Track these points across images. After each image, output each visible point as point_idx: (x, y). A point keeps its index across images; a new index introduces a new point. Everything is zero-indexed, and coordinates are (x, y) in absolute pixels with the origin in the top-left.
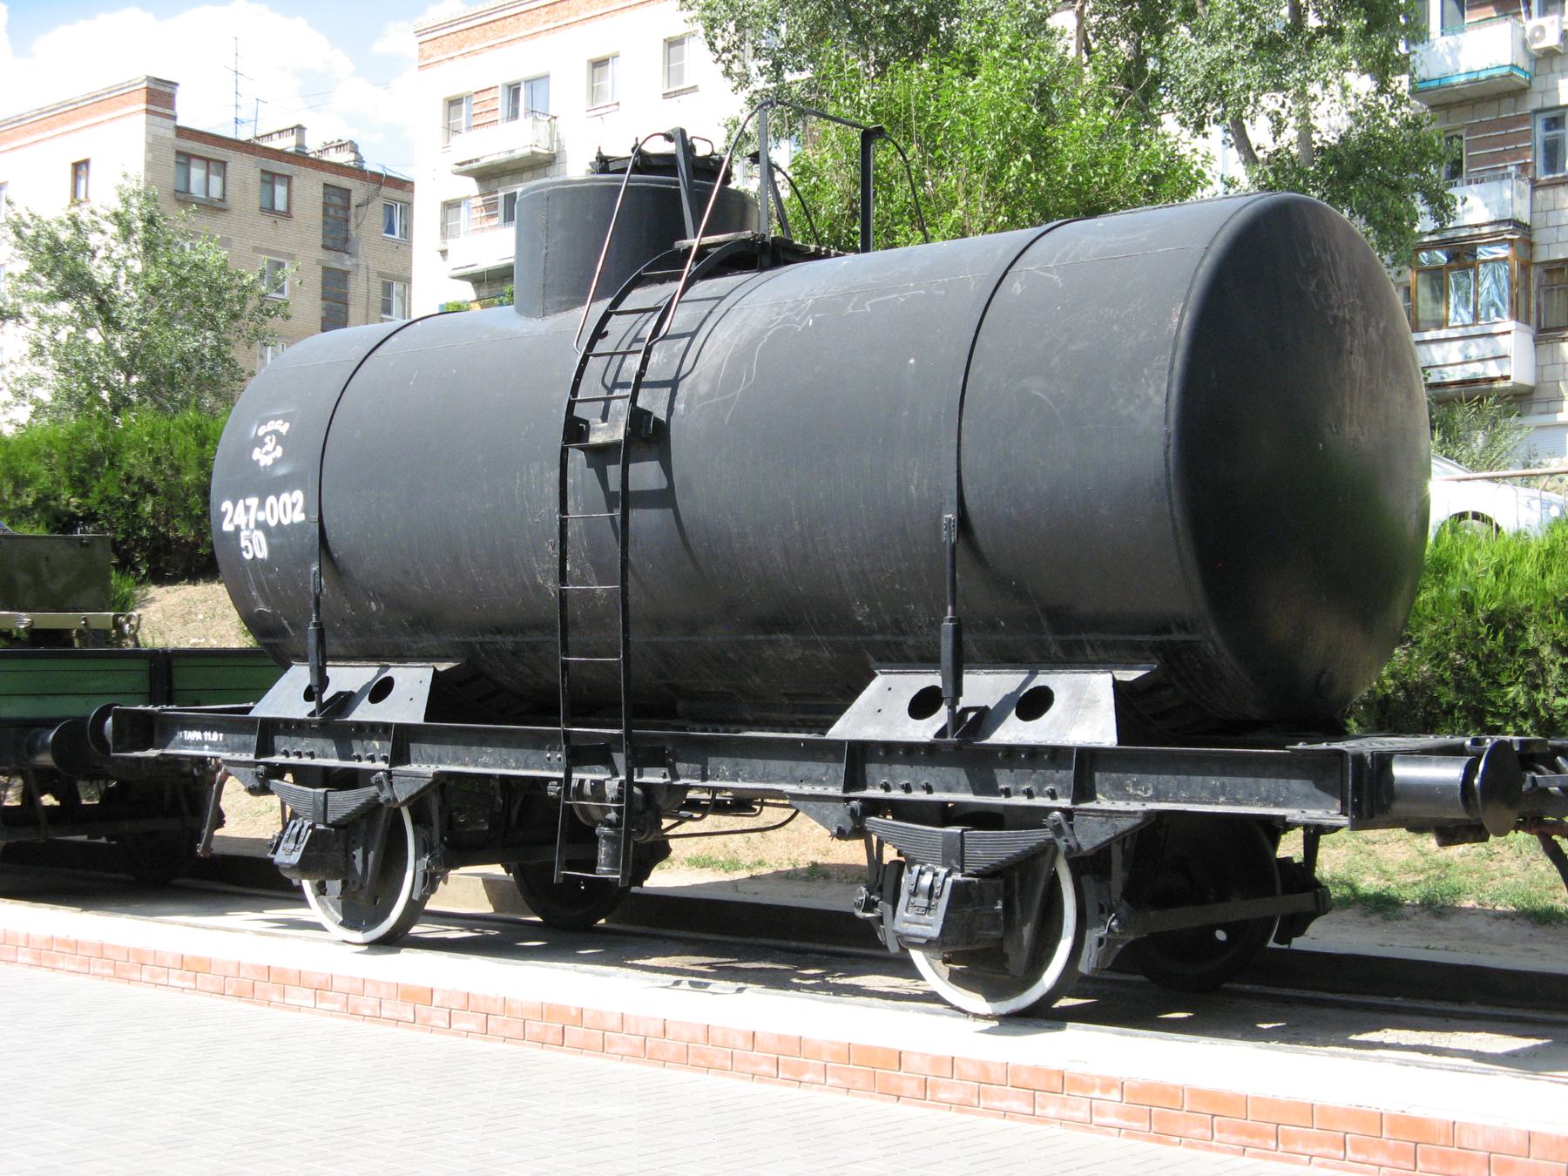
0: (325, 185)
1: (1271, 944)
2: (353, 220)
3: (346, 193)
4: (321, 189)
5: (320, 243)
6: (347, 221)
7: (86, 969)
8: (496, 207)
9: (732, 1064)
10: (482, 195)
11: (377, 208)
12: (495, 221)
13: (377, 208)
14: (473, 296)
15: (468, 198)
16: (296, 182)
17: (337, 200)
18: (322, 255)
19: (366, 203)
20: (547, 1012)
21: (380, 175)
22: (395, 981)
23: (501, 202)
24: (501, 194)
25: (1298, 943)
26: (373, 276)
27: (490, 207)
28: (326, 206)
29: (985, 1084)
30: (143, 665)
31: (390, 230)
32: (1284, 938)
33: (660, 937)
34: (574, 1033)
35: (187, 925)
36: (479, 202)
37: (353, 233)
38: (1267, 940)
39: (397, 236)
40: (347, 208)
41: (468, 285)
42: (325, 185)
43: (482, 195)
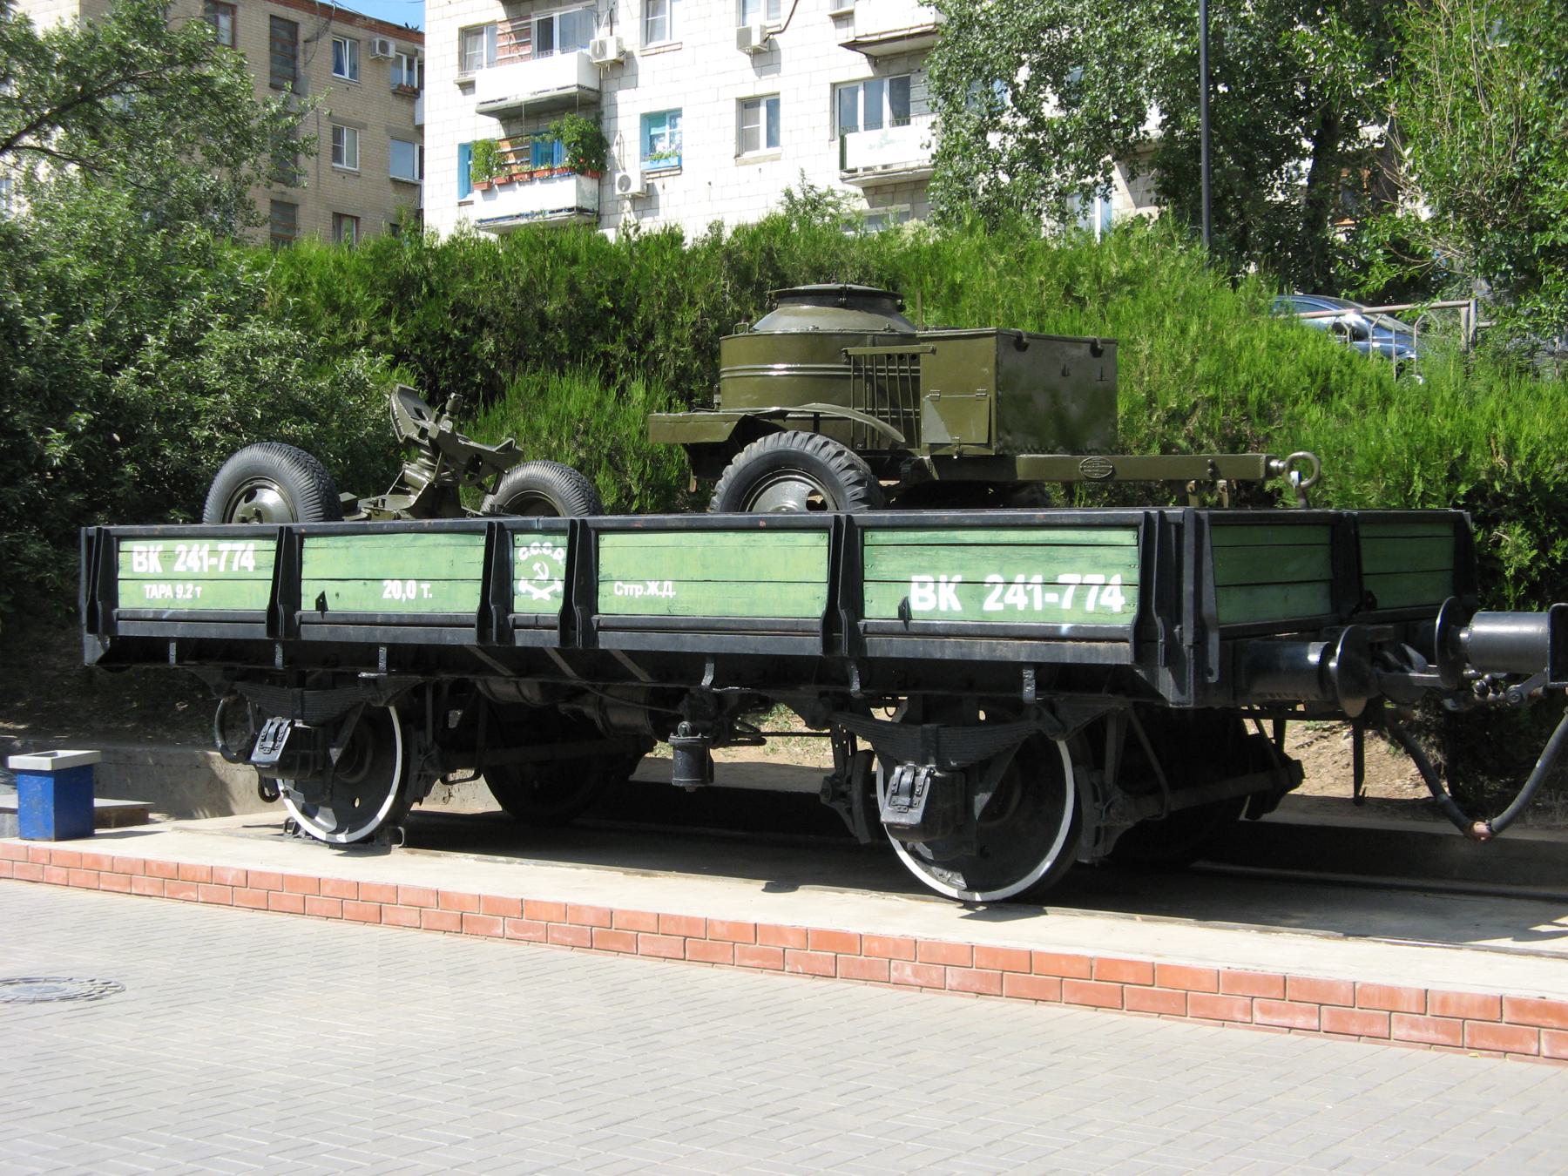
0: (272, 17)
1: (1242, 817)
2: (301, 57)
3: (293, 27)
4: (267, 21)
5: (267, 82)
6: (295, 58)
7: (1314, 1023)
8: (528, 34)
9: (777, 963)
10: (510, 20)
11: (326, 43)
12: (526, 51)
13: (326, 43)
14: (502, 135)
15: (494, 23)
16: (240, 11)
17: (284, 34)
18: (556, 52)
19: (317, 37)
20: (1357, 995)
21: (330, 8)
22: (435, 888)
23: (534, 29)
24: (535, 20)
25: (1266, 817)
26: (323, 121)
27: (521, 35)
28: (273, 38)
29: (303, 897)
30: (1322, 535)
31: (339, 69)
32: (1254, 812)
33: (1518, 896)
34: (315, 902)
35: (1538, 954)
36: (508, 28)
37: (302, 71)
38: (1238, 814)
39: (347, 76)
40: (295, 43)
41: (494, 121)
42: (272, 17)
43: (510, 20)
